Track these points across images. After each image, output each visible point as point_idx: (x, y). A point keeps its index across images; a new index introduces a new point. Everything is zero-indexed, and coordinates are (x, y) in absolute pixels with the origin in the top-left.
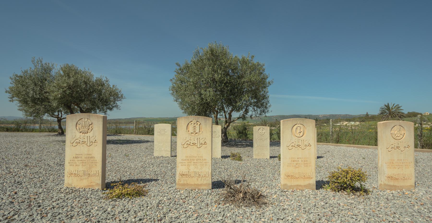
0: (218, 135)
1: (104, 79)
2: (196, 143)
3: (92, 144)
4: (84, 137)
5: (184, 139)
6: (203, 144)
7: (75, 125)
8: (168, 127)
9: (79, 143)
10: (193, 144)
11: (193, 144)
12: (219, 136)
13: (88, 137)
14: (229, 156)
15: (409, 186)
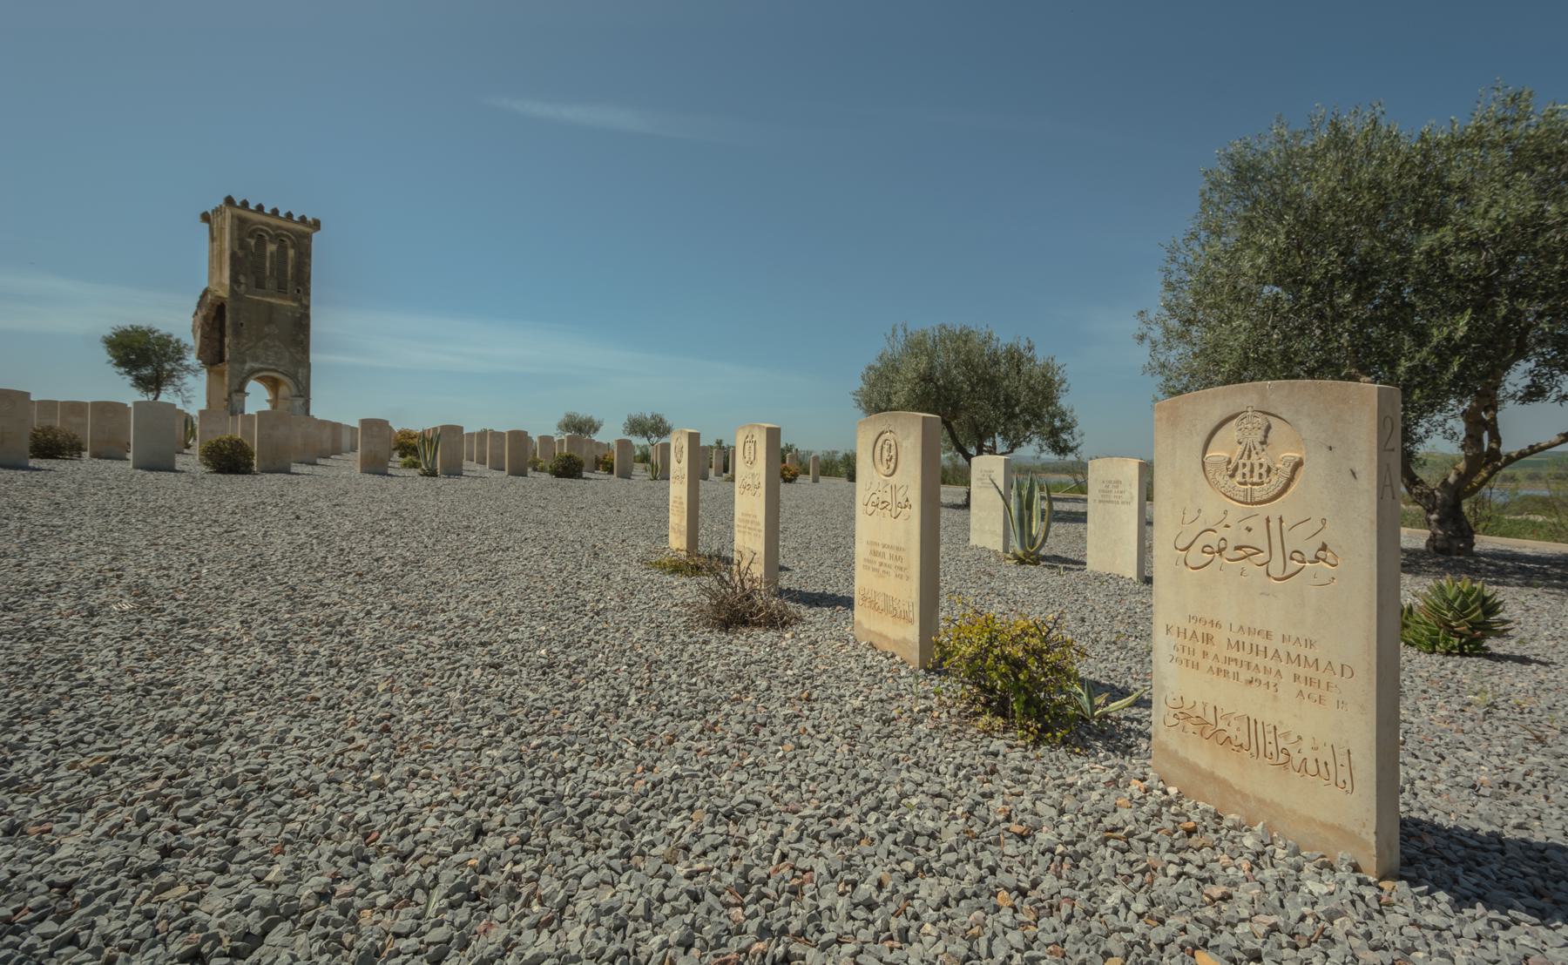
0: (1126, 496)
1: (1023, 344)
2: (889, 500)
3: (1297, 565)
4: (1250, 523)
5: (1187, 520)
6: (1309, 555)
7: (1204, 436)
8: (960, 500)
9: (1220, 551)
10: (1238, 548)
11: (1238, 548)
12: (1132, 498)
13: (1274, 525)
14: (947, 506)
15: (1323, 825)
